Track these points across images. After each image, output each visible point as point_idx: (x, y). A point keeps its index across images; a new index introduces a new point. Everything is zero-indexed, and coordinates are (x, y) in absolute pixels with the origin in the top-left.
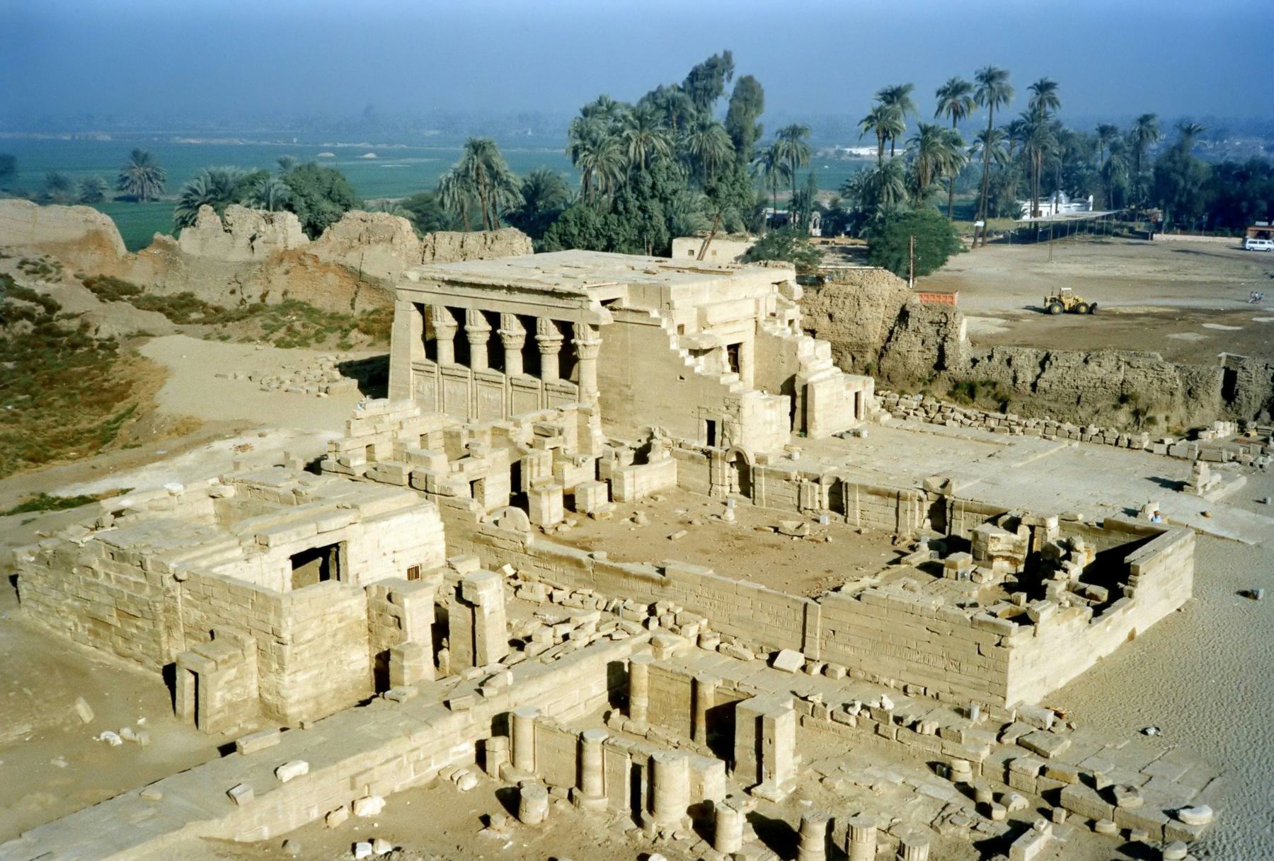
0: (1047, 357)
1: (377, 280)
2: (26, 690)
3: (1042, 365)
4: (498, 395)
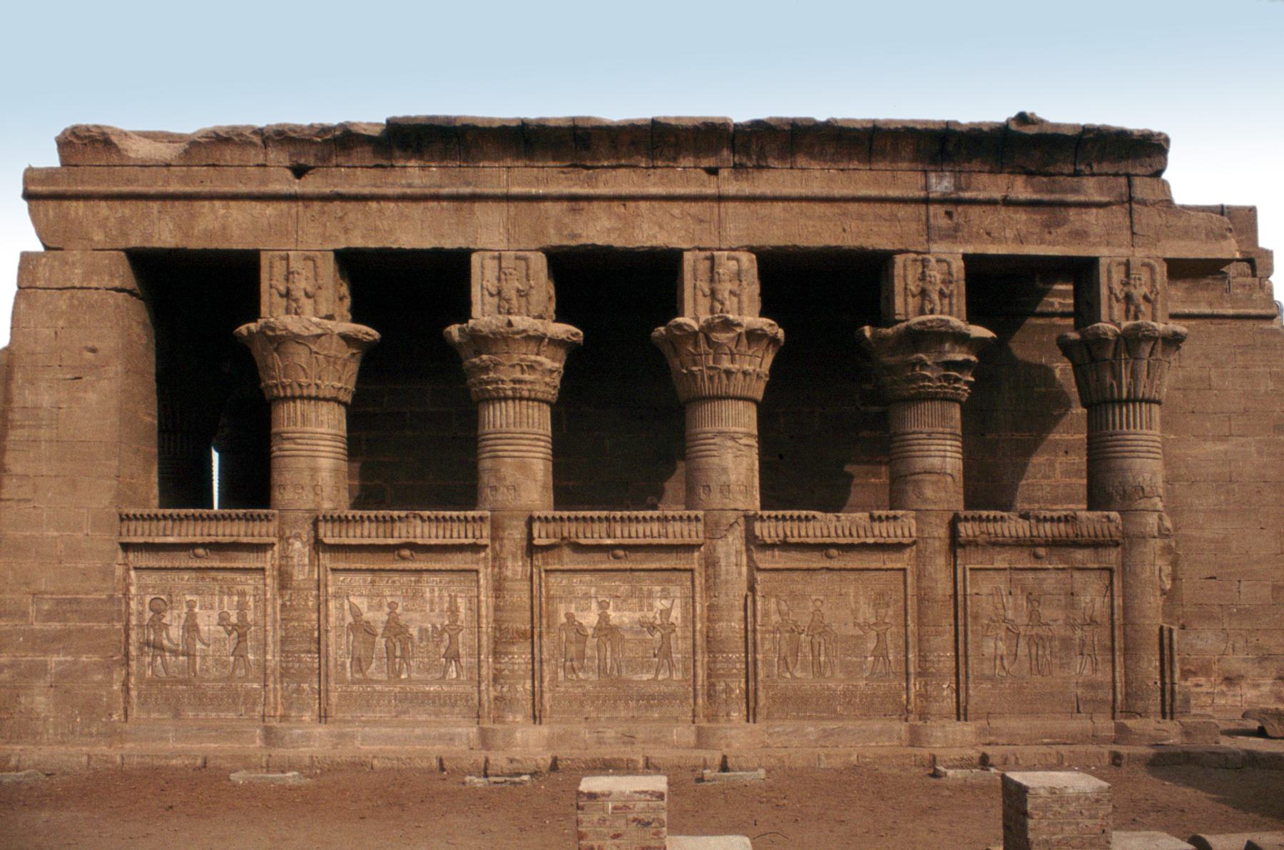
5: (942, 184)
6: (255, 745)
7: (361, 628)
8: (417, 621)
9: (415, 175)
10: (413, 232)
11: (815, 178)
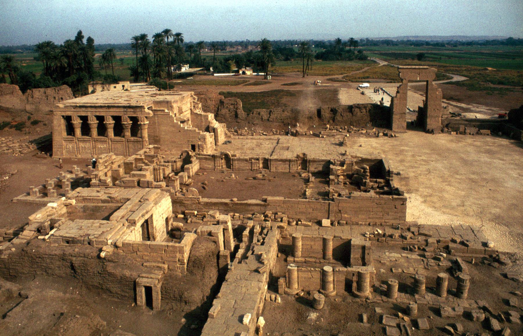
0: (271, 111)
1: (8, 108)
2: (77, 316)
3: (270, 114)
4: (105, 146)
5: (125, 110)
6: (74, 156)
7: (82, 147)
8: (86, 147)
9: (84, 109)
10: (83, 114)
11: (115, 109)
